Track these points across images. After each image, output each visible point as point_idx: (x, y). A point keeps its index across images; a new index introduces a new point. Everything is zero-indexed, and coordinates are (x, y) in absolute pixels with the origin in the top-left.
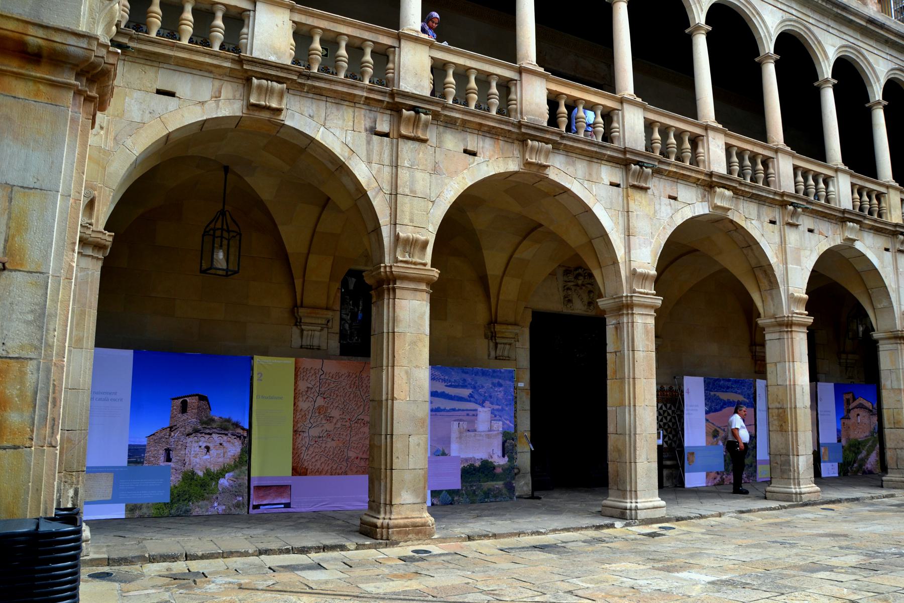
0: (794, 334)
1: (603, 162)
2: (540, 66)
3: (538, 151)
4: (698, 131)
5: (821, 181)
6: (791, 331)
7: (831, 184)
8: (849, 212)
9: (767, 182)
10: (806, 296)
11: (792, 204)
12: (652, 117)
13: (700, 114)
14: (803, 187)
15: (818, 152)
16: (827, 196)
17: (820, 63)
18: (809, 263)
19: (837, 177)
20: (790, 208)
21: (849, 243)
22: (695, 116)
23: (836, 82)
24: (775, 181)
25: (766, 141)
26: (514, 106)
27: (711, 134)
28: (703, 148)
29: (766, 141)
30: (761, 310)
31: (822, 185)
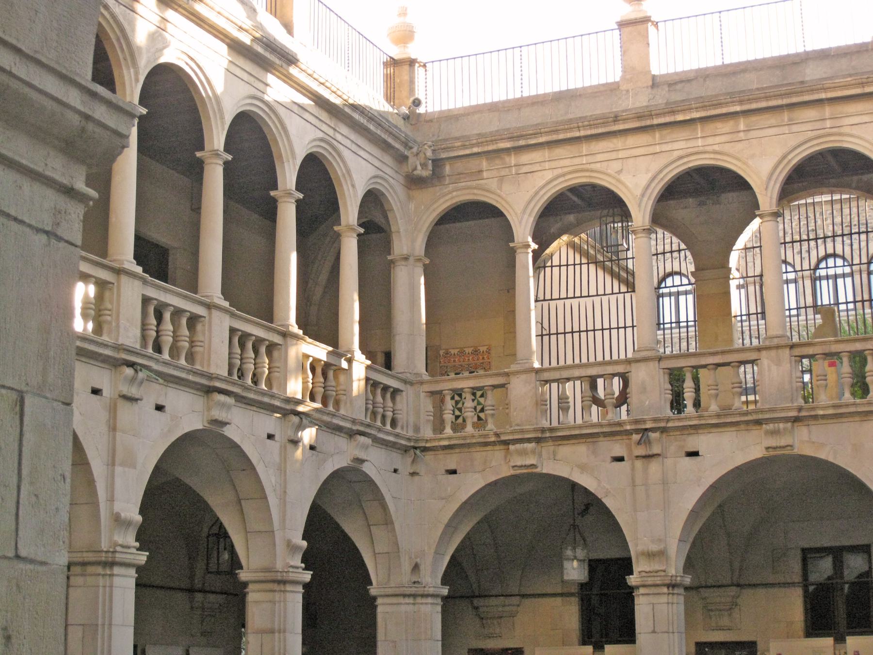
0: (115, 579)
1: (342, 435)
2: (139, 263)
3: (223, 405)
4: (199, 310)
5: (249, 345)
6: (112, 575)
7: (199, 327)
8: (218, 378)
9: (191, 357)
10: (140, 518)
11: (131, 365)
12: (151, 293)
13: (111, 250)
14: (187, 345)
15: (265, 309)
16: (158, 337)
17: (209, 118)
18: (148, 459)
19: (119, 281)
20: (129, 371)
21: (356, 465)
22: (104, 254)
23: (301, 196)
24: (110, 323)
25: (271, 321)
26: (109, 318)
27: (216, 313)
28: (111, 303)
29: (271, 321)
30: (243, 562)
31: (185, 331)
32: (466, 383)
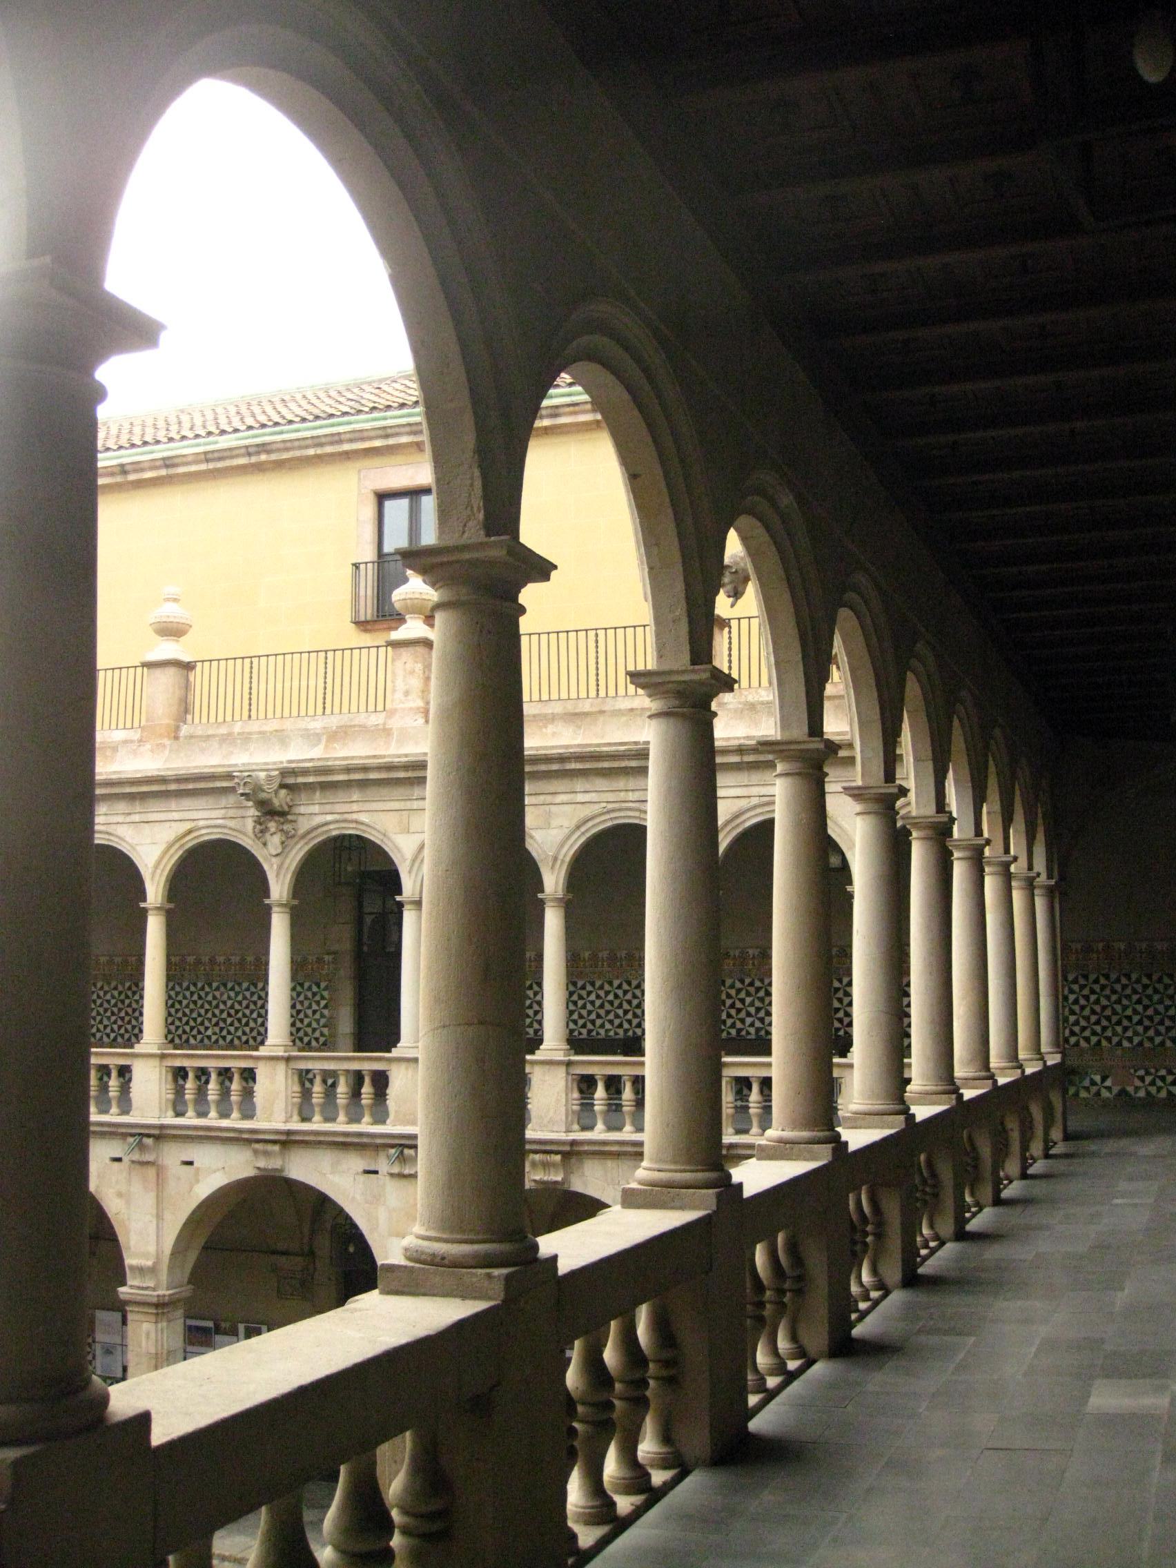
32: (213, 1060)
